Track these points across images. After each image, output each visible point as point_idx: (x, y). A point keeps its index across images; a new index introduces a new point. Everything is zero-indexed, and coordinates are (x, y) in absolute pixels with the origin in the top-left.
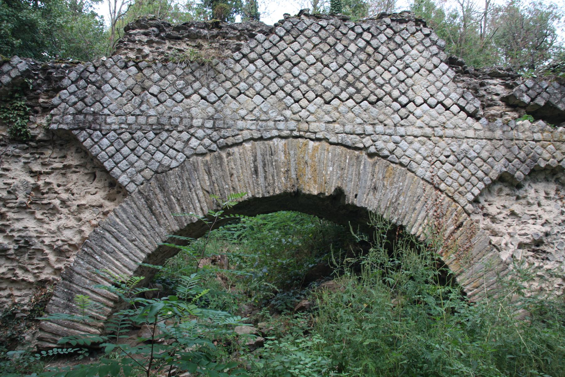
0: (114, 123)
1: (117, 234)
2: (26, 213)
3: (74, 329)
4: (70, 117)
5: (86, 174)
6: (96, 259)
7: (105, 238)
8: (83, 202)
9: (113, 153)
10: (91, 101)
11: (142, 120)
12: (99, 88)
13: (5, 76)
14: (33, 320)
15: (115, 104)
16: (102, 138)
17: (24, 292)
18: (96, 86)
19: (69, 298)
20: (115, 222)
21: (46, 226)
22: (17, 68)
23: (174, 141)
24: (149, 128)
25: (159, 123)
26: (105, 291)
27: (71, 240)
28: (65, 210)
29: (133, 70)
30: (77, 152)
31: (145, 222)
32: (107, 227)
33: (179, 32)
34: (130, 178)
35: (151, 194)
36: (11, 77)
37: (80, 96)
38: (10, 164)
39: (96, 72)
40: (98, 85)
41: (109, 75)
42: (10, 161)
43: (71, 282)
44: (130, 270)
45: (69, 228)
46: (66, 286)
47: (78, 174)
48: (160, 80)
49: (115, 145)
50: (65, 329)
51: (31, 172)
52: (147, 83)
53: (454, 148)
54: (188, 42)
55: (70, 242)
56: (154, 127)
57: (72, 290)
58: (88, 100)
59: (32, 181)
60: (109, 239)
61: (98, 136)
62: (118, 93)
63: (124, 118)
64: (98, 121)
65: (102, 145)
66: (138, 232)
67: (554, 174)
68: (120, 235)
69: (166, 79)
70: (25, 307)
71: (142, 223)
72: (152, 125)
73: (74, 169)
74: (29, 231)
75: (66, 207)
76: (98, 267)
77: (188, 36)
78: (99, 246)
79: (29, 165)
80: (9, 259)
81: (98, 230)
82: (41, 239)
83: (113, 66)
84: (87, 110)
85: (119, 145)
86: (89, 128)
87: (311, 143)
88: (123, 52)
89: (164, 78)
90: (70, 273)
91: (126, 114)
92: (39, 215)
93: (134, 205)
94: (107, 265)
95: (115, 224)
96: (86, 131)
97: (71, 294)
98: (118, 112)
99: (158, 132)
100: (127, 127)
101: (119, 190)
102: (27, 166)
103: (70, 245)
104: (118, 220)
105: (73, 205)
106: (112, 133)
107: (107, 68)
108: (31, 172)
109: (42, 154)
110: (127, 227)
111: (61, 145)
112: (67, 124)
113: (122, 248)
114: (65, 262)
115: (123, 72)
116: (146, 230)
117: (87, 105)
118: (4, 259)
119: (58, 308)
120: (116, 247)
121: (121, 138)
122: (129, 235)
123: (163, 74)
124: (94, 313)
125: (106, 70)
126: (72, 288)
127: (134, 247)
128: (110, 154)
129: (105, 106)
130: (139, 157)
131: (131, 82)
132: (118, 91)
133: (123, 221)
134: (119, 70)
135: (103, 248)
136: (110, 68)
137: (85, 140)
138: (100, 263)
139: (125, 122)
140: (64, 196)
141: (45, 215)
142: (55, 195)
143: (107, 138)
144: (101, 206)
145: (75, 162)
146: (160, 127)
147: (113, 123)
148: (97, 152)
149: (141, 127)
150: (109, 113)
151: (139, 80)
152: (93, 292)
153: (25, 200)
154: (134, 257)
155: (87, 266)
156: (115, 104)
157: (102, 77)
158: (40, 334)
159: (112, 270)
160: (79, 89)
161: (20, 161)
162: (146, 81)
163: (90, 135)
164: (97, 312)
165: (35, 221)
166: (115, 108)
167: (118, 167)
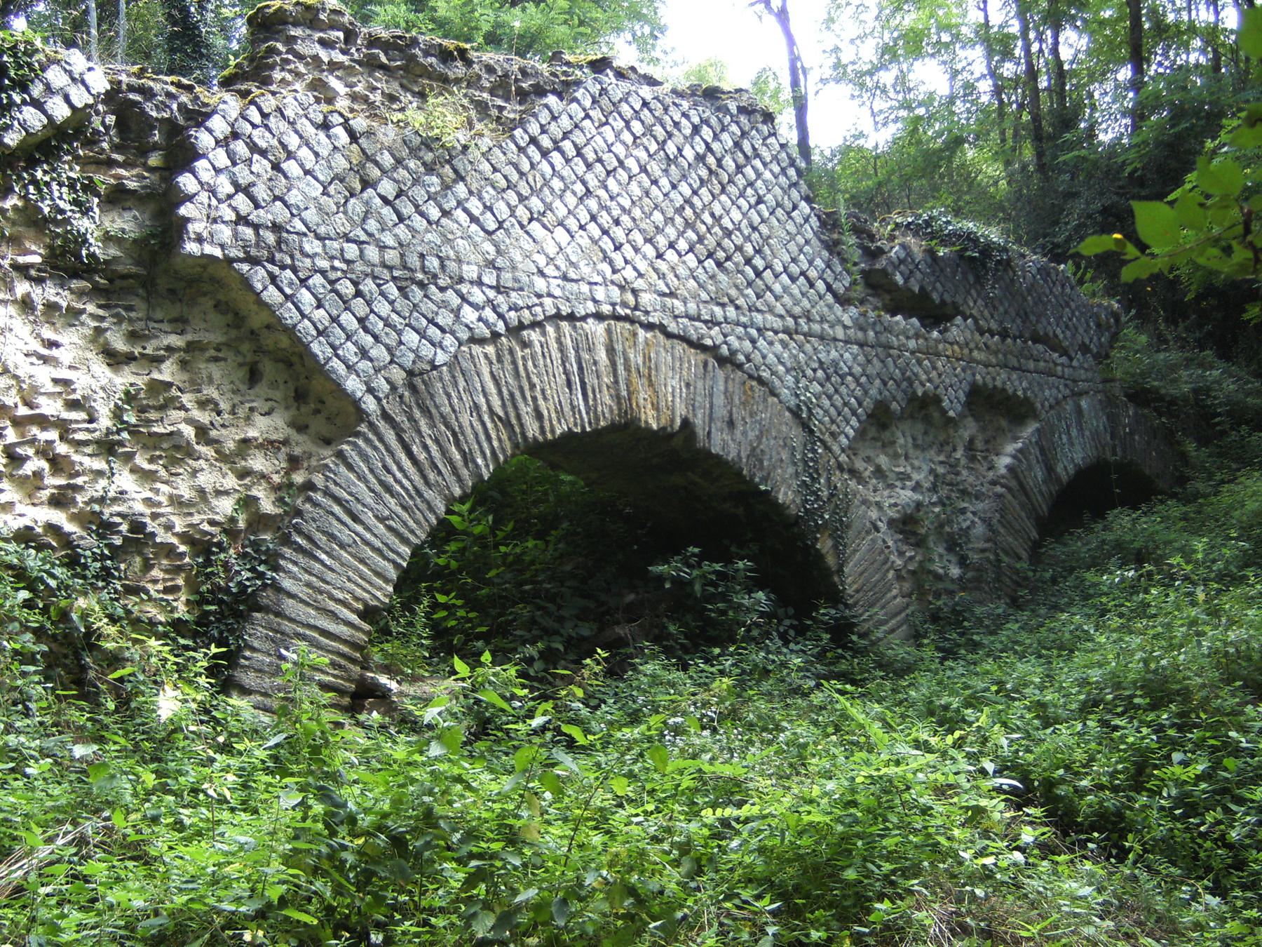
4: (225, 233)
5: (240, 365)
10: (266, 198)
23: (435, 309)
24: (386, 274)
38: (56, 330)
47: (222, 363)
48: (395, 169)
53: (822, 356)
54: (405, 81)
56: (396, 273)
67: (921, 408)
82: (163, 520)
84: (258, 216)
86: (272, 261)
87: (641, 333)
92: (141, 461)
96: (264, 267)
100: (344, 267)
101: (319, 406)
104: (352, 476)
111: (172, 291)
113: (368, 536)
129: (295, 212)
130: (376, 338)
131: (340, 163)
132: (316, 179)
137: (265, 288)
140: (204, 417)
142: (182, 414)
146: (407, 274)
150: (305, 230)
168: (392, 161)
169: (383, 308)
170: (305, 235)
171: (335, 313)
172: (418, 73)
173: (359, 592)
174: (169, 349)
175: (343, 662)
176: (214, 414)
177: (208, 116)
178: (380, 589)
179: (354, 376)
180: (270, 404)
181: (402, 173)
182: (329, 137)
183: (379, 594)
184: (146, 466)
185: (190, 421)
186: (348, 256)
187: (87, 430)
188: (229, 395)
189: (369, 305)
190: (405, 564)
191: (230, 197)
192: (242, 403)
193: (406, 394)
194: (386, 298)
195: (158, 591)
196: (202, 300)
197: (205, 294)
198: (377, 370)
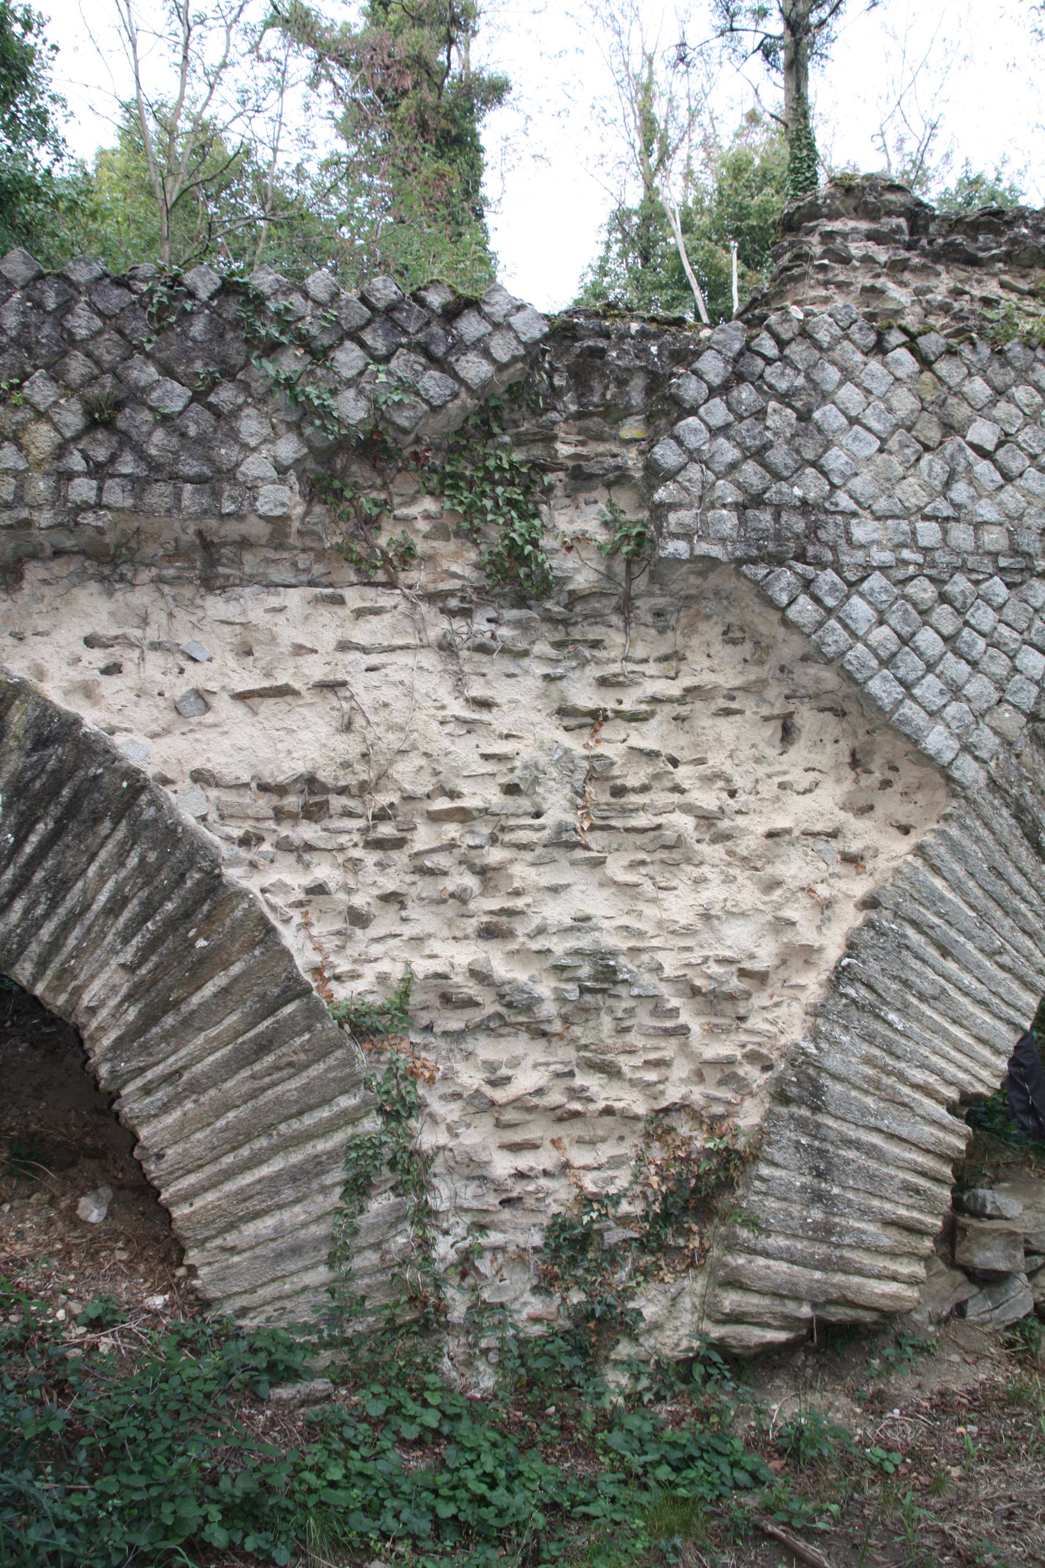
0: (878, 542)
1: (946, 934)
2: (573, 863)
3: (845, 1272)
4: (727, 521)
5: (766, 719)
6: (890, 1024)
7: (908, 948)
8: (781, 822)
9: (894, 648)
10: (790, 462)
11: (961, 535)
12: (805, 416)
13: (472, 356)
14: (663, 1248)
15: (866, 475)
16: (848, 597)
17: (606, 1151)
18: (793, 408)
19: (817, 1168)
20: (933, 890)
21: (651, 911)
22: (510, 327)
25: (1015, 551)
26: (928, 1133)
27: (752, 957)
28: (715, 852)
29: (904, 360)
30: (729, 638)
31: (1026, 889)
32: (911, 908)
33: (976, 240)
34: (959, 737)
35: (1027, 791)
36: (494, 361)
37: (749, 442)
38: (488, 683)
39: (783, 358)
40: (798, 404)
41: (833, 374)
42: (491, 671)
43: (816, 1109)
44: (997, 1052)
45: (743, 914)
46: (802, 1124)
47: (738, 717)
48: (994, 403)
49: (894, 619)
50: (818, 1275)
51: (564, 712)
52: (960, 412)
54: (1006, 278)
55: (747, 965)
56: (1003, 562)
57: (824, 1140)
58: (779, 456)
59: (576, 744)
60: (921, 951)
61: (833, 587)
62: (871, 437)
63: (904, 525)
64: (822, 535)
65: (855, 620)
66: (1008, 922)
68: (953, 934)
69: (1011, 400)
70: (625, 1207)
71: (1016, 892)
72: (995, 555)
73: (722, 703)
74: (599, 929)
75: (714, 841)
76: (899, 1052)
77: (1007, 258)
78: (894, 978)
79: (563, 684)
80: (544, 1034)
81: (884, 919)
82: (645, 958)
83: (837, 340)
84: (779, 492)
85: (906, 621)
86: (801, 557)
88: (812, 293)
89: (1000, 393)
90: (810, 1078)
91: (906, 514)
93: (984, 833)
94: (926, 1043)
95: (933, 900)
96: (790, 568)
97: (822, 1153)
98: (881, 505)
99: (1018, 579)
100: (919, 558)
101: (890, 775)
102: (554, 688)
103: (743, 973)
104: (938, 883)
105: (744, 831)
106: (876, 581)
107: (817, 345)
108: (564, 712)
109: (596, 644)
110: (973, 907)
112: (723, 540)
113: (967, 979)
114: (744, 1038)
115: (874, 365)
116: (1030, 915)
117: (777, 477)
118: (524, 1036)
119: (784, 1205)
120: (948, 979)
121: (906, 597)
122: (983, 934)
123: (998, 381)
124: (903, 1212)
125: (816, 354)
126: (823, 1131)
127: (1002, 975)
128: (884, 654)
129: (837, 481)
130: (973, 664)
132: (869, 429)
133: (957, 887)
134: (859, 357)
135: (905, 983)
136: (830, 349)
137: (792, 601)
138: (903, 1034)
139: (912, 540)
140: (709, 799)
141: (643, 870)
142: (676, 798)
143: (862, 595)
144: (834, 835)
145: (729, 679)
146: (1019, 562)
147: (873, 542)
148: (843, 646)
149: (964, 561)
150: (853, 507)
151: (929, 398)
152: (892, 1136)
153: (571, 818)
154: (1004, 1008)
155: (865, 1048)
156: (866, 475)
157: (808, 377)
158: (730, 1300)
159: (943, 1057)
160: (741, 418)
161: (527, 672)
162: (952, 400)
163: (807, 585)
164: (908, 1207)
165: (606, 892)
166: (871, 490)
167: (914, 699)
168: (989, 391)
169: (984, 617)
170: (854, 514)
171: (906, 631)
172: (1027, 262)
173: (951, 1070)
174: (654, 700)
175: (923, 1183)
176: (725, 795)
177: (697, 354)
178: (985, 1065)
179: (940, 728)
180: (813, 776)
181: (1002, 409)
182: (885, 365)
183: (984, 1074)
184: (624, 877)
185: (688, 809)
186: (923, 542)
187: (531, 827)
188: (750, 766)
189: (959, 612)
190: (1027, 1025)
191: (733, 466)
192: (769, 776)
193: (1027, 750)
194: (988, 602)
195: (635, 1068)
196: (703, 626)
197: (708, 617)
198: (980, 716)
